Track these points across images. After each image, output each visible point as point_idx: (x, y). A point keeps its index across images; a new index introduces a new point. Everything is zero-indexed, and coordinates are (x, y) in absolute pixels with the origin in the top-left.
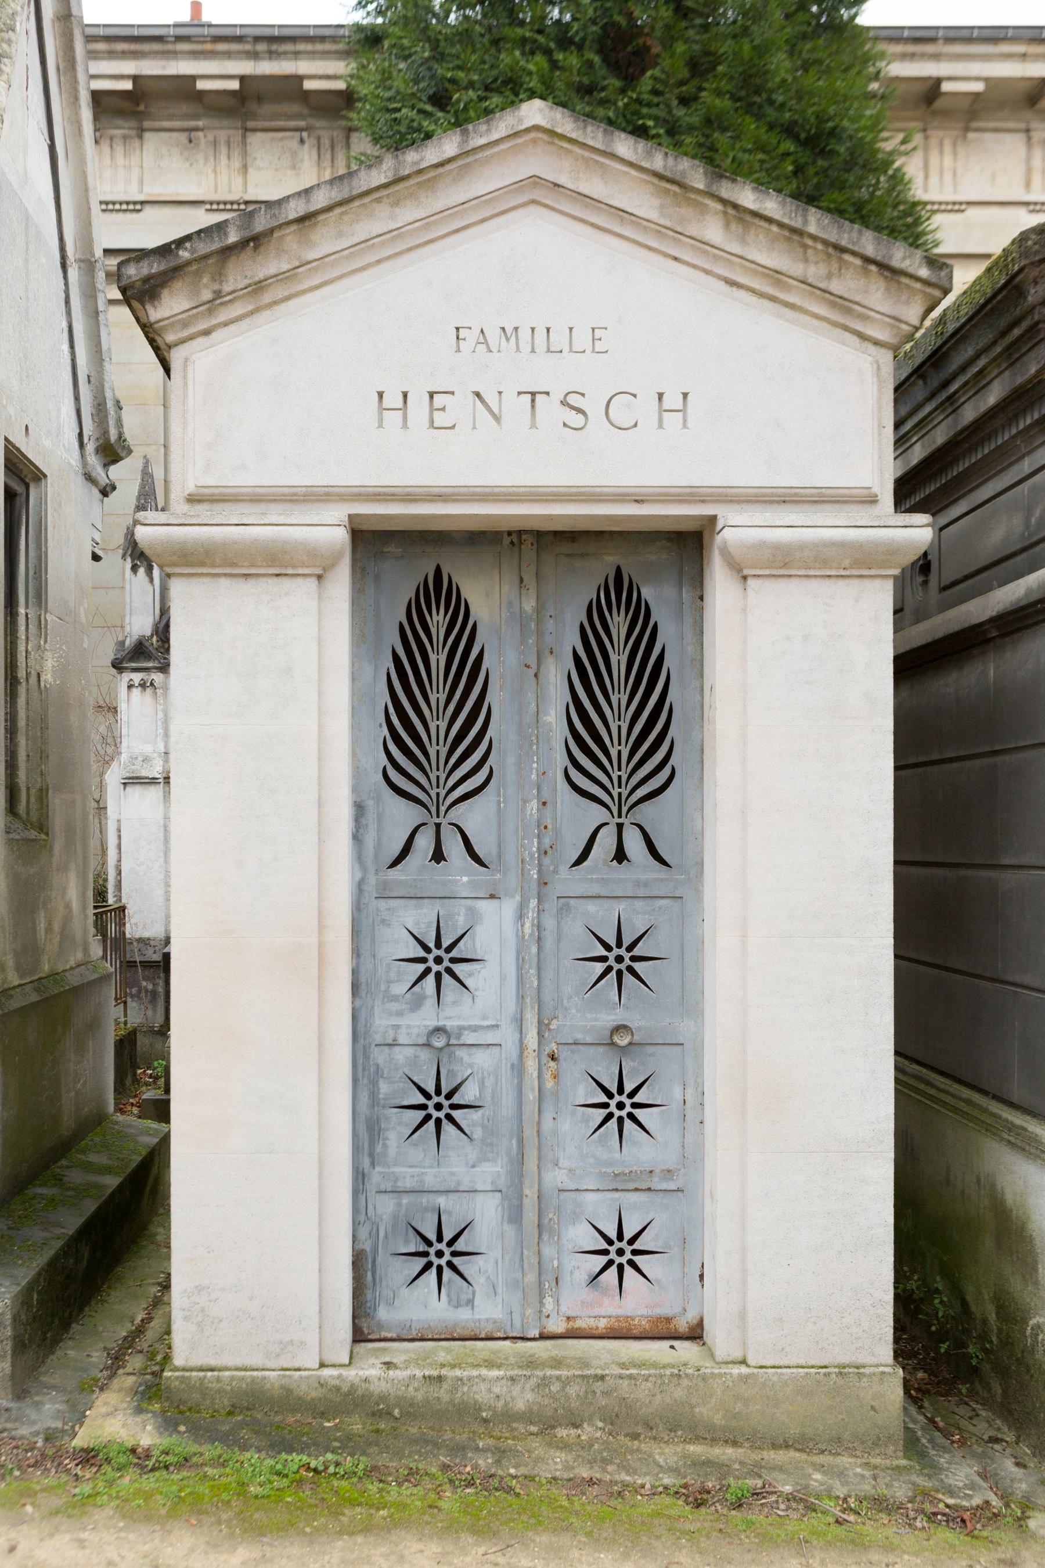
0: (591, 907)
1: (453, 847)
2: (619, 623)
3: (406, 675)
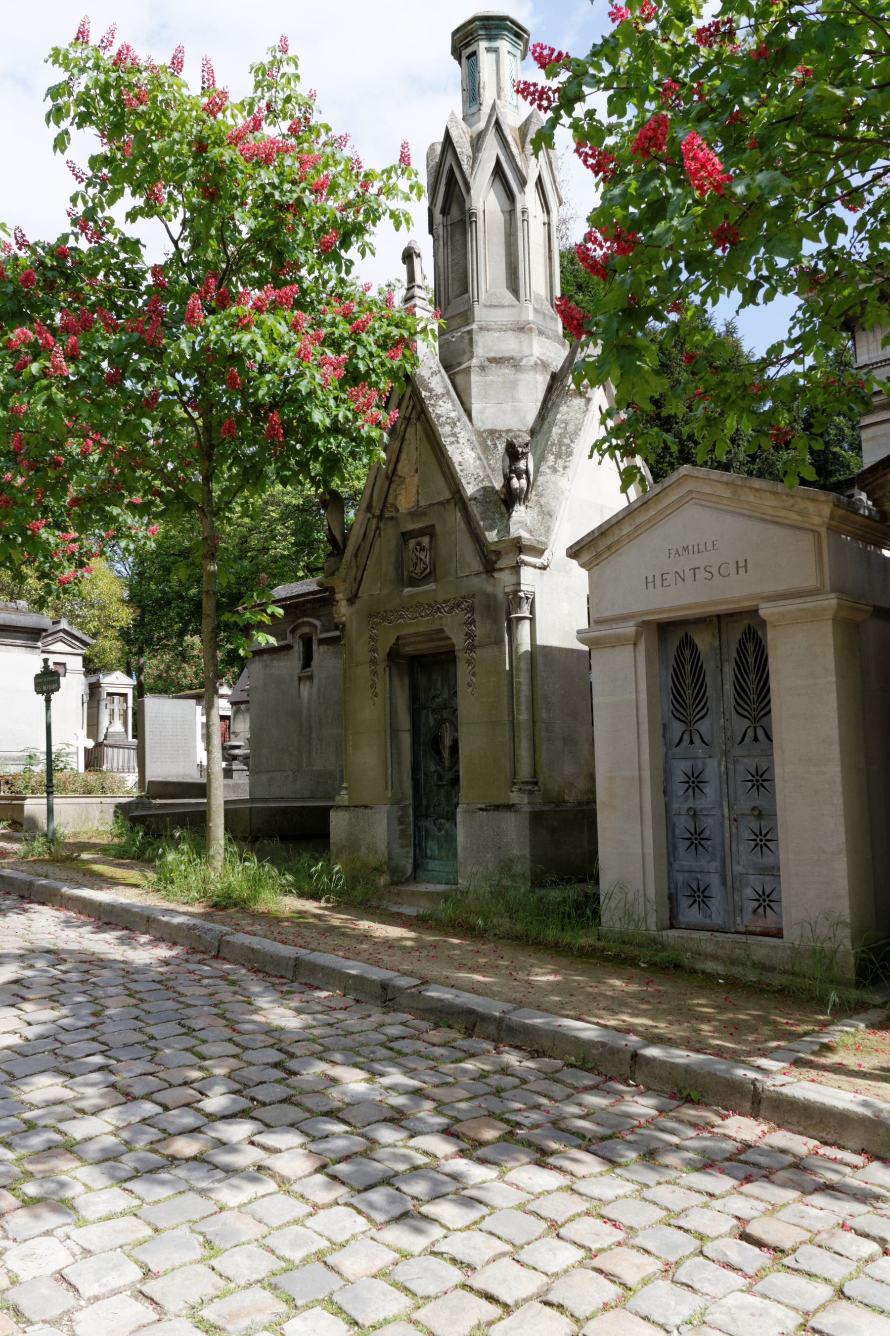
0: (746, 760)
1: (697, 739)
2: (750, 646)
3: (678, 675)
